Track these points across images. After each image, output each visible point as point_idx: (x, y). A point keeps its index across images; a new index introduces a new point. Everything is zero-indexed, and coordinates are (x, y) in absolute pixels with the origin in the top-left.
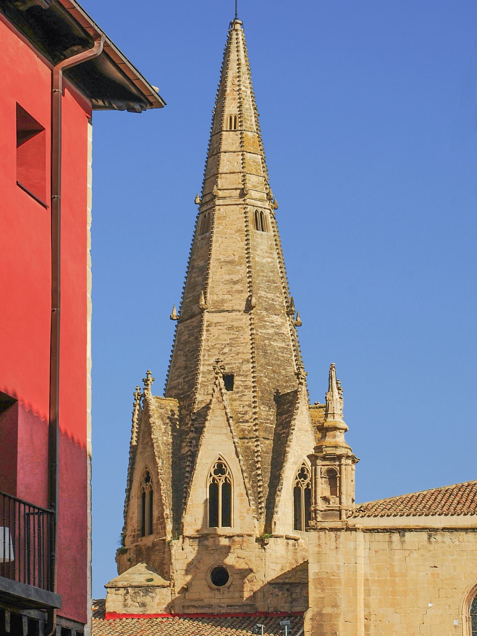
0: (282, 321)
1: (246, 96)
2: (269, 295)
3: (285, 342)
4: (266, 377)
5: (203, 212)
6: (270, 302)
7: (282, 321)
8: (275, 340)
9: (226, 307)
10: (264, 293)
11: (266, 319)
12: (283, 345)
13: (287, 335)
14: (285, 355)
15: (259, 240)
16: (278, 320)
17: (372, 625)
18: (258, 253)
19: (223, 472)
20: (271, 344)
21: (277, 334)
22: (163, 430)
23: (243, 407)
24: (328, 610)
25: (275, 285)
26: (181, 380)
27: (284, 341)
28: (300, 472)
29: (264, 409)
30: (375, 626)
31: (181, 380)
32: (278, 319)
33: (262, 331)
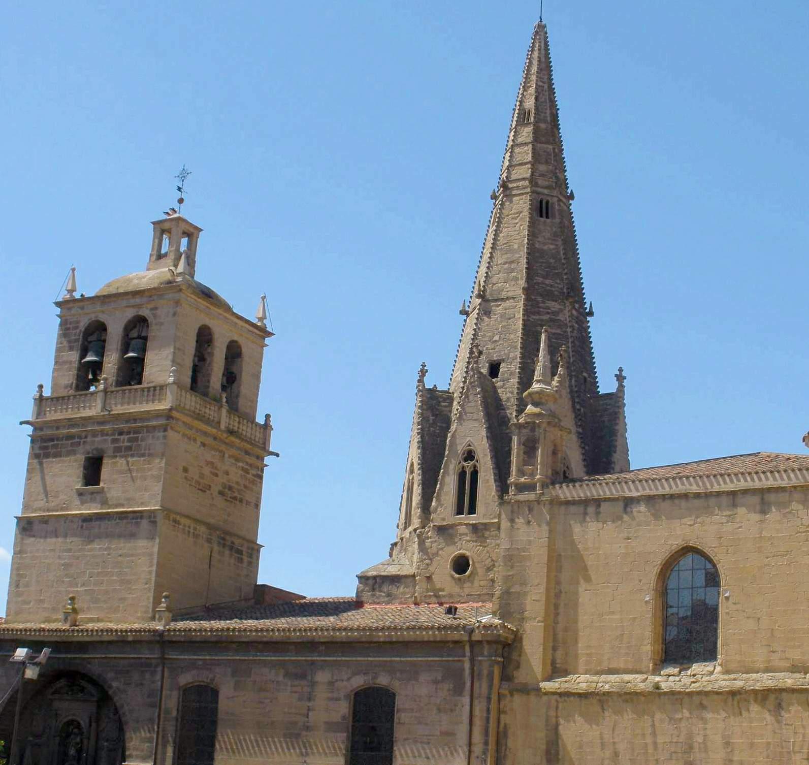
3: (561, 329)
6: (548, 288)
7: (559, 307)
9: (504, 294)
10: (541, 279)
12: (558, 331)
13: (565, 322)
15: (542, 227)
16: (554, 306)
17: (562, 605)
18: (538, 240)
22: (431, 421)
23: (506, 394)
24: (516, 589)
25: (557, 271)
27: (559, 327)
33: (534, 317)
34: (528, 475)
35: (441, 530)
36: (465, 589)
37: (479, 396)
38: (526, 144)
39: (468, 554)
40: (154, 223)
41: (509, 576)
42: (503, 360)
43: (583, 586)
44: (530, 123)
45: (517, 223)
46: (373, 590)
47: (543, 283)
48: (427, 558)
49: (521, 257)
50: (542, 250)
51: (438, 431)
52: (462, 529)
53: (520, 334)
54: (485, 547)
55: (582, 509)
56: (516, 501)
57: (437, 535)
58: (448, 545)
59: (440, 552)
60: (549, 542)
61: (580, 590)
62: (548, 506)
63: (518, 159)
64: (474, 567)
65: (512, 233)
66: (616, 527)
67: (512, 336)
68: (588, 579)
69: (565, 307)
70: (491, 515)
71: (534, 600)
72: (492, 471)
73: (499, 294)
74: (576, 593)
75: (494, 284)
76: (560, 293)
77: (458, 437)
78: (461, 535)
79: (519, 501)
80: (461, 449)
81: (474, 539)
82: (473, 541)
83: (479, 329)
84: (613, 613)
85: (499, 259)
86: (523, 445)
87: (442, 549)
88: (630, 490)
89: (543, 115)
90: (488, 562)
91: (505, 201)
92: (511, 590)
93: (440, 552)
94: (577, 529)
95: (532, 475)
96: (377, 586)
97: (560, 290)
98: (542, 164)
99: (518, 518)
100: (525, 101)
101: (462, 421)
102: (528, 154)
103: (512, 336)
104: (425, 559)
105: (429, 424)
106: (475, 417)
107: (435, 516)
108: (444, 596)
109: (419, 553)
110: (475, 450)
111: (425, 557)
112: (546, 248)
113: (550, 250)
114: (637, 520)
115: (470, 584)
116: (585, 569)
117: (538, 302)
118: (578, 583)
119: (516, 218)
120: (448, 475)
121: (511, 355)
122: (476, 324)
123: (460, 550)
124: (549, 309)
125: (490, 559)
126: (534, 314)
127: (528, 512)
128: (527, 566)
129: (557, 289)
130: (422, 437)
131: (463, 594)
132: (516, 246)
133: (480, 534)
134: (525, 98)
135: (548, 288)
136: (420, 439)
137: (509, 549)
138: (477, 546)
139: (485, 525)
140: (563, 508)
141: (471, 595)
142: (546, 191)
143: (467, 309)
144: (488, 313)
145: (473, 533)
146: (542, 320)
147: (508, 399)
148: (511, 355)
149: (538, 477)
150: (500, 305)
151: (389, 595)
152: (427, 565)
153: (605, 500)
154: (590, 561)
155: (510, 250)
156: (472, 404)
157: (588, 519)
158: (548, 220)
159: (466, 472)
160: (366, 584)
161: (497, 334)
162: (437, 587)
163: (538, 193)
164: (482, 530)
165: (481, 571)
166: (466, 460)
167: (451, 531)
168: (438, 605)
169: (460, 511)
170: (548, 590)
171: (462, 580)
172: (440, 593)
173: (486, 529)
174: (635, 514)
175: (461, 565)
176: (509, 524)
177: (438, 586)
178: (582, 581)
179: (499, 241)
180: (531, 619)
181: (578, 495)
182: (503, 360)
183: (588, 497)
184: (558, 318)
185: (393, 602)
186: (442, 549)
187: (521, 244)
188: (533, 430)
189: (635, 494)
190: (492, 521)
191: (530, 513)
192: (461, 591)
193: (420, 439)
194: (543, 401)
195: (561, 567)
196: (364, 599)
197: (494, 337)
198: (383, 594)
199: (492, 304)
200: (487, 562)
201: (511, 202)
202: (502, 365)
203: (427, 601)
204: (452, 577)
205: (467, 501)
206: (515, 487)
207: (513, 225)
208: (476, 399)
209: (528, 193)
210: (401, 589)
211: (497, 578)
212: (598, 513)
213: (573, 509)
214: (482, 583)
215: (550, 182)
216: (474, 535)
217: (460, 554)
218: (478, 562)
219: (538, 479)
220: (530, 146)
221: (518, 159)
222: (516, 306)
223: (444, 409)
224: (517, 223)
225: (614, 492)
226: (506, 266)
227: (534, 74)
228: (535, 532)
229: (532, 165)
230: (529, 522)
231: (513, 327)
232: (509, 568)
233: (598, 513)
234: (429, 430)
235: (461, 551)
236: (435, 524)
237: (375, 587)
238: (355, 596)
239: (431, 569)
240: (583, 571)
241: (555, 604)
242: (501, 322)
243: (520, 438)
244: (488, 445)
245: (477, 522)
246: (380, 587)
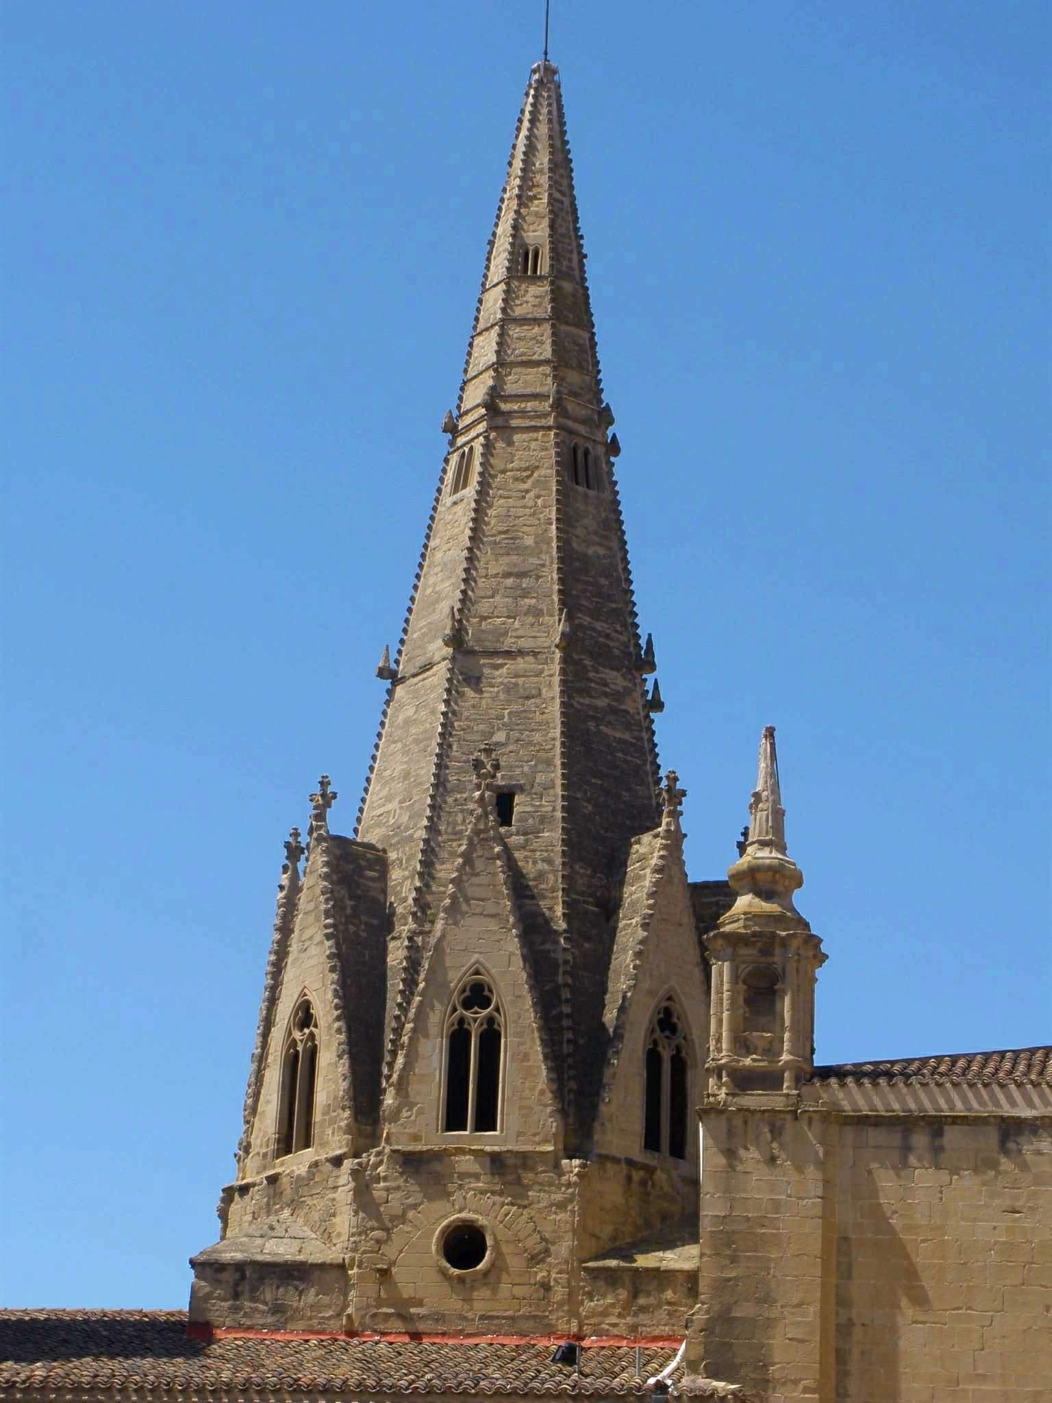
0: (626, 684)
1: (562, 210)
2: (599, 625)
3: (632, 731)
4: (588, 801)
5: (459, 448)
7: (626, 684)
8: (609, 722)
9: (508, 643)
10: (588, 619)
11: (591, 675)
12: (627, 736)
14: (629, 758)
15: (580, 505)
17: (856, 1352)
19: (485, 1003)
20: (599, 732)
21: (614, 711)
23: (535, 863)
25: (614, 606)
26: (394, 805)
27: (628, 727)
28: (662, 1016)
29: (582, 871)
30: (862, 1353)
31: (394, 805)
32: (616, 678)
33: (582, 700)
34: (760, 1050)
35: (412, 1163)
36: (476, 1305)
37: (499, 863)
38: (536, 321)
39: (482, 1220)
40: (193, 1263)
41: (729, 1280)
42: (521, 788)
43: (908, 1311)
44: (541, 278)
45: (527, 491)
46: (236, 1296)
47: (594, 629)
48: (376, 1225)
49: (543, 565)
50: (585, 555)
51: (364, 935)
52: (466, 1163)
53: (557, 732)
54: (525, 1207)
55: (896, 1138)
56: (739, 1110)
57: (402, 1174)
58: (430, 1198)
59: (411, 1214)
60: (824, 1206)
61: (900, 1321)
62: (817, 1125)
63: (518, 350)
64: (499, 1253)
65: (521, 511)
66: (984, 1184)
67: (537, 737)
68: (920, 1299)
69: (635, 685)
70: (535, 1135)
71: (790, 1339)
72: (536, 1034)
73: (498, 641)
74: (893, 1330)
75: (483, 618)
76: (622, 652)
77: (448, 951)
78: (462, 1176)
79: (748, 1110)
80: (456, 977)
81: (497, 1188)
82: (493, 1193)
83: (454, 713)
84: (983, 1378)
85: (491, 564)
86: (744, 982)
87: (415, 1206)
88: (1013, 1103)
89: (565, 263)
90: (533, 1243)
91: (495, 439)
92: (733, 1314)
93: (411, 1214)
94: (886, 1181)
95: (772, 1051)
96: (245, 1288)
97: (622, 648)
98: (573, 368)
99: (746, 1149)
100: (525, 227)
101: (459, 917)
102: (542, 343)
103: (537, 737)
104: (373, 1229)
105: (347, 917)
106: (490, 908)
107: (393, 1130)
108: (422, 1318)
109: (356, 1213)
110: (492, 983)
111: (373, 1223)
112: (590, 551)
113: (598, 557)
114: (1034, 1171)
115: (488, 1292)
116: (912, 1273)
117: (585, 667)
118: (895, 1305)
119: (523, 481)
120: (427, 1036)
121: (540, 778)
122: (447, 702)
123: (460, 1211)
124: (606, 685)
125: (537, 1237)
126: (581, 692)
127: (769, 1136)
128: (772, 1259)
129: (616, 644)
130: (338, 945)
131: (470, 1315)
132: (529, 541)
133: (510, 1178)
134: (524, 220)
135: (601, 639)
136: (334, 950)
137: (725, 1217)
138: (503, 1204)
139: (524, 1156)
140: (849, 1134)
141: (491, 1318)
142: (582, 429)
143: (393, 666)
144: (474, 680)
145: (493, 1174)
146: (596, 708)
147: (541, 876)
148: (540, 778)
149: (785, 1057)
150: (502, 666)
151: (277, 1309)
152: (378, 1241)
153: (955, 1120)
154: (922, 1257)
155: (513, 546)
156: (483, 879)
157: (912, 1160)
158: (591, 493)
159: (467, 1035)
160: (217, 1282)
161: (499, 729)
162: (405, 1296)
163: (571, 432)
164: (516, 1167)
165: (515, 1263)
166: (467, 1004)
167: (437, 1167)
168: (407, 1339)
169: (454, 1120)
170: (823, 1316)
171: (468, 1281)
172: (412, 1310)
173: (525, 1166)
174: (1029, 1157)
175: (464, 1246)
176: (722, 1161)
177: (407, 1292)
178: (904, 1302)
179: (488, 524)
180: (785, 1383)
181: (853, 1102)
182: (521, 788)
183: (910, 1111)
184: (623, 707)
185: (289, 1326)
186: (415, 1206)
187: (542, 539)
188: (766, 952)
189: (1026, 1113)
190: (538, 1149)
191: (773, 1139)
192: (466, 1307)
193: (334, 950)
194: (780, 888)
195: (850, 1266)
196: (213, 1317)
197: (493, 734)
198: (261, 1307)
199: (482, 661)
200: (530, 1243)
201: (510, 443)
202: (517, 799)
203: (381, 1327)
204: (443, 1273)
205: (471, 1094)
206: (728, 1075)
207: (520, 494)
208: (490, 869)
209: (549, 428)
210: (311, 1296)
211: (555, 1280)
212: (937, 1150)
213: (874, 1136)
214: (519, 1291)
215: (590, 412)
216: (497, 1179)
217: (463, 1221)
218: (507, 1242)
219: (786, 1062)
220: (547, 329)
221: (518, 350)
222: (542, 672)
223: (371, 884)
224: (527, 491)
225: (975, 1105)
226: (510, 581)
227: (541, 171)
228: (789, 1183)
229: (555, 369)
230: (772, 1160)
231: (538, 717)
232: (728, 1262)
233: (937, 1150)
234: (347, 930)
235: (464, 1215)
236: (396, 1147)
237: (240, 1289)
238: (186, 1309)
239: (390, 1251)
240: (906, 1281)
241: (837, 1350)
242: (509, 702)
243: (737, 968)
244: (525, 976)
245: (504, 1149)
246: (254, 1289)
